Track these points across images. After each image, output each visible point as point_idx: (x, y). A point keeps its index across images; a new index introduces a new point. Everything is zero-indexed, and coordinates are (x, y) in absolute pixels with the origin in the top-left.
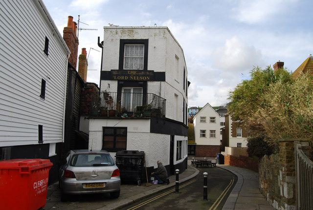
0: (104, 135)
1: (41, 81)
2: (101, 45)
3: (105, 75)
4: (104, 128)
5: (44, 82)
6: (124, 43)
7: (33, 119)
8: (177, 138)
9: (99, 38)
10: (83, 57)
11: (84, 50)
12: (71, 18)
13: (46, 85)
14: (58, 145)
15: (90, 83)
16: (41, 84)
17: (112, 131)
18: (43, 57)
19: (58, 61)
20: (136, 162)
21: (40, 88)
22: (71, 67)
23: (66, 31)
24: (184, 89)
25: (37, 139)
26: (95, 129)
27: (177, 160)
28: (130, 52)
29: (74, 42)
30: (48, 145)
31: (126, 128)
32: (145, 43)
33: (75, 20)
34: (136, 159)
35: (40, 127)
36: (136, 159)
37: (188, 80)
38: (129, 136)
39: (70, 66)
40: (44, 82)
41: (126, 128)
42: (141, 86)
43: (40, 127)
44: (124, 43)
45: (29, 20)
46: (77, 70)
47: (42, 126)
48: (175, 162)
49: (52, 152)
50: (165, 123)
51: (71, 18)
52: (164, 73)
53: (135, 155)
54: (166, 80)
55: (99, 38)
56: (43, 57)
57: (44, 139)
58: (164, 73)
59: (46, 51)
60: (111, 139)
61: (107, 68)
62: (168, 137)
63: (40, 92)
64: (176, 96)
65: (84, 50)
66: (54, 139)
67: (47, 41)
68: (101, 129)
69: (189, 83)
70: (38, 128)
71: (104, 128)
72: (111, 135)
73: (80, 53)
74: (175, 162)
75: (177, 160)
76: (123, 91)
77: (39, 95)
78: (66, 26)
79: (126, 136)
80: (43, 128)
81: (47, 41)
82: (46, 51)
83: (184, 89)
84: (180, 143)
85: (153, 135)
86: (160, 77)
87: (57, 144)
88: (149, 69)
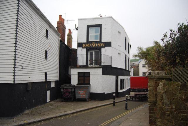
0: (79, 77)
1: (45, 51)
2: (77, 29)
3: (80, 45)
4: (79, 73)
5: (46, 52)
6: (89, 27)
7: (42, 70)
8: (120, 77)
9: (76, 25)
10: (70, 35)
11: (70, 30)
12: (60, 16)
13: (48, 53)
14: (56, 82)
15: (73, 49)
16: (45, 53)
17: (83, 75)
18: (46, 40)
19: (54, 42)
20: (71, 90)
21: (45, 55)
22: (62, 42)
23: (59, 23)
24: (126, 49)
25: (44, 79)
26: (74, 73)
27: (121, 89)
28: (92, 32)
29: (63, 28)
30: (50, 82)
31: (89, 73)
32: (100, 26)
33: (63, 17)
34: (71, 89)
35: (46, 74)
36: (71, 89)
37: (130, 44)
38: (92, 78)
39: (60, 41)
40: (46, 52)
41: (89, 73)
42: (98, 50)
43: (46, 74)
44: (89, 27)
45: (34, 31)
46: (66, 43)
47: (46, 73)
48: (120, 91)
49: (53, 85)
50: (111, 70)
51: (60, 16)
52: (110, 42)
53: (66, 86)
54: (112, 46)
55: (76, 25)
56: (46, 40)
57: (47, 79)
58: (110, 42)
59: (47, 36)
60: (82, 78)
61: (80, 42)
62: (113, 78)
63: (45, 56)
64: (119, 54)
65: (70, 30)
66: (54, 79)
67: (47, 31)
68: (77, 73)
69: (130, 46)
70: (44, 74)
71: (79, 73)
72: (86, 76)
73: (67, 32)
74: (120, 91)
75: (121, 89)
76: (89, 53)
77: (45, 36)
78: (58, 20)
79: (89, 77)
80: (47, 74)
81: (47, 31)
82: (47, 36)
83: (126, 49)
84: (122, 81)
85: (104, 76)
86: (109, 44)
87: (55, 81)
88: (102, 41)
